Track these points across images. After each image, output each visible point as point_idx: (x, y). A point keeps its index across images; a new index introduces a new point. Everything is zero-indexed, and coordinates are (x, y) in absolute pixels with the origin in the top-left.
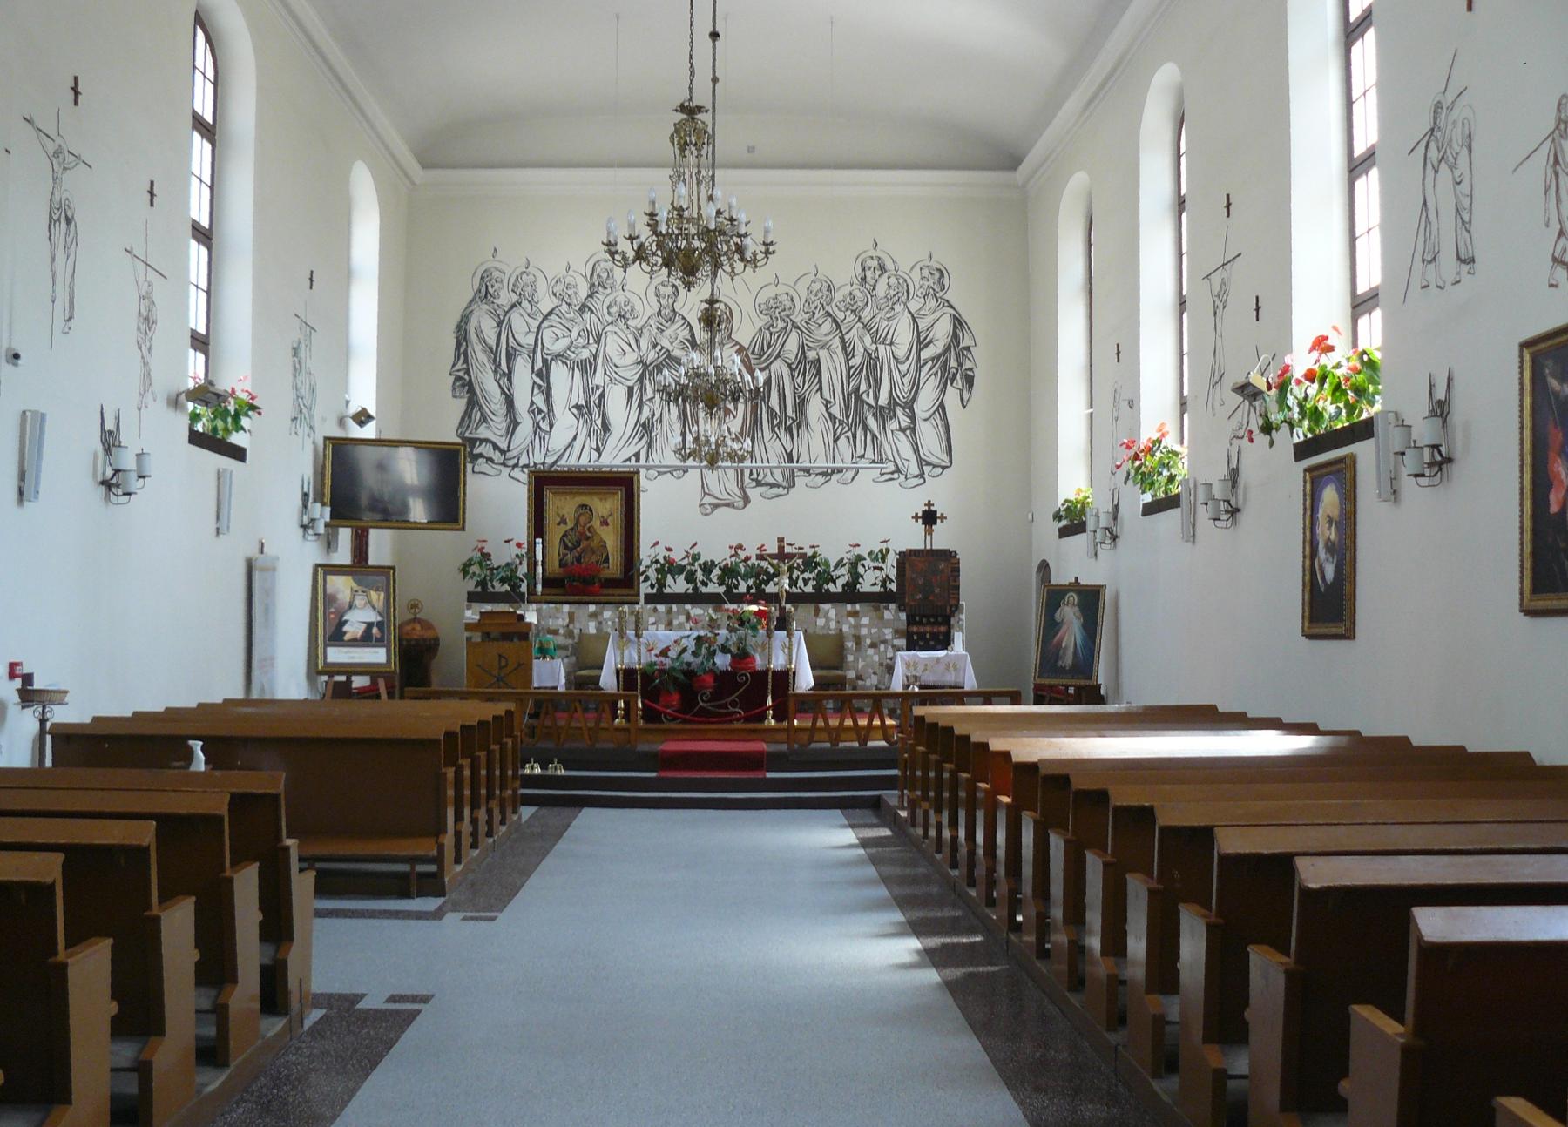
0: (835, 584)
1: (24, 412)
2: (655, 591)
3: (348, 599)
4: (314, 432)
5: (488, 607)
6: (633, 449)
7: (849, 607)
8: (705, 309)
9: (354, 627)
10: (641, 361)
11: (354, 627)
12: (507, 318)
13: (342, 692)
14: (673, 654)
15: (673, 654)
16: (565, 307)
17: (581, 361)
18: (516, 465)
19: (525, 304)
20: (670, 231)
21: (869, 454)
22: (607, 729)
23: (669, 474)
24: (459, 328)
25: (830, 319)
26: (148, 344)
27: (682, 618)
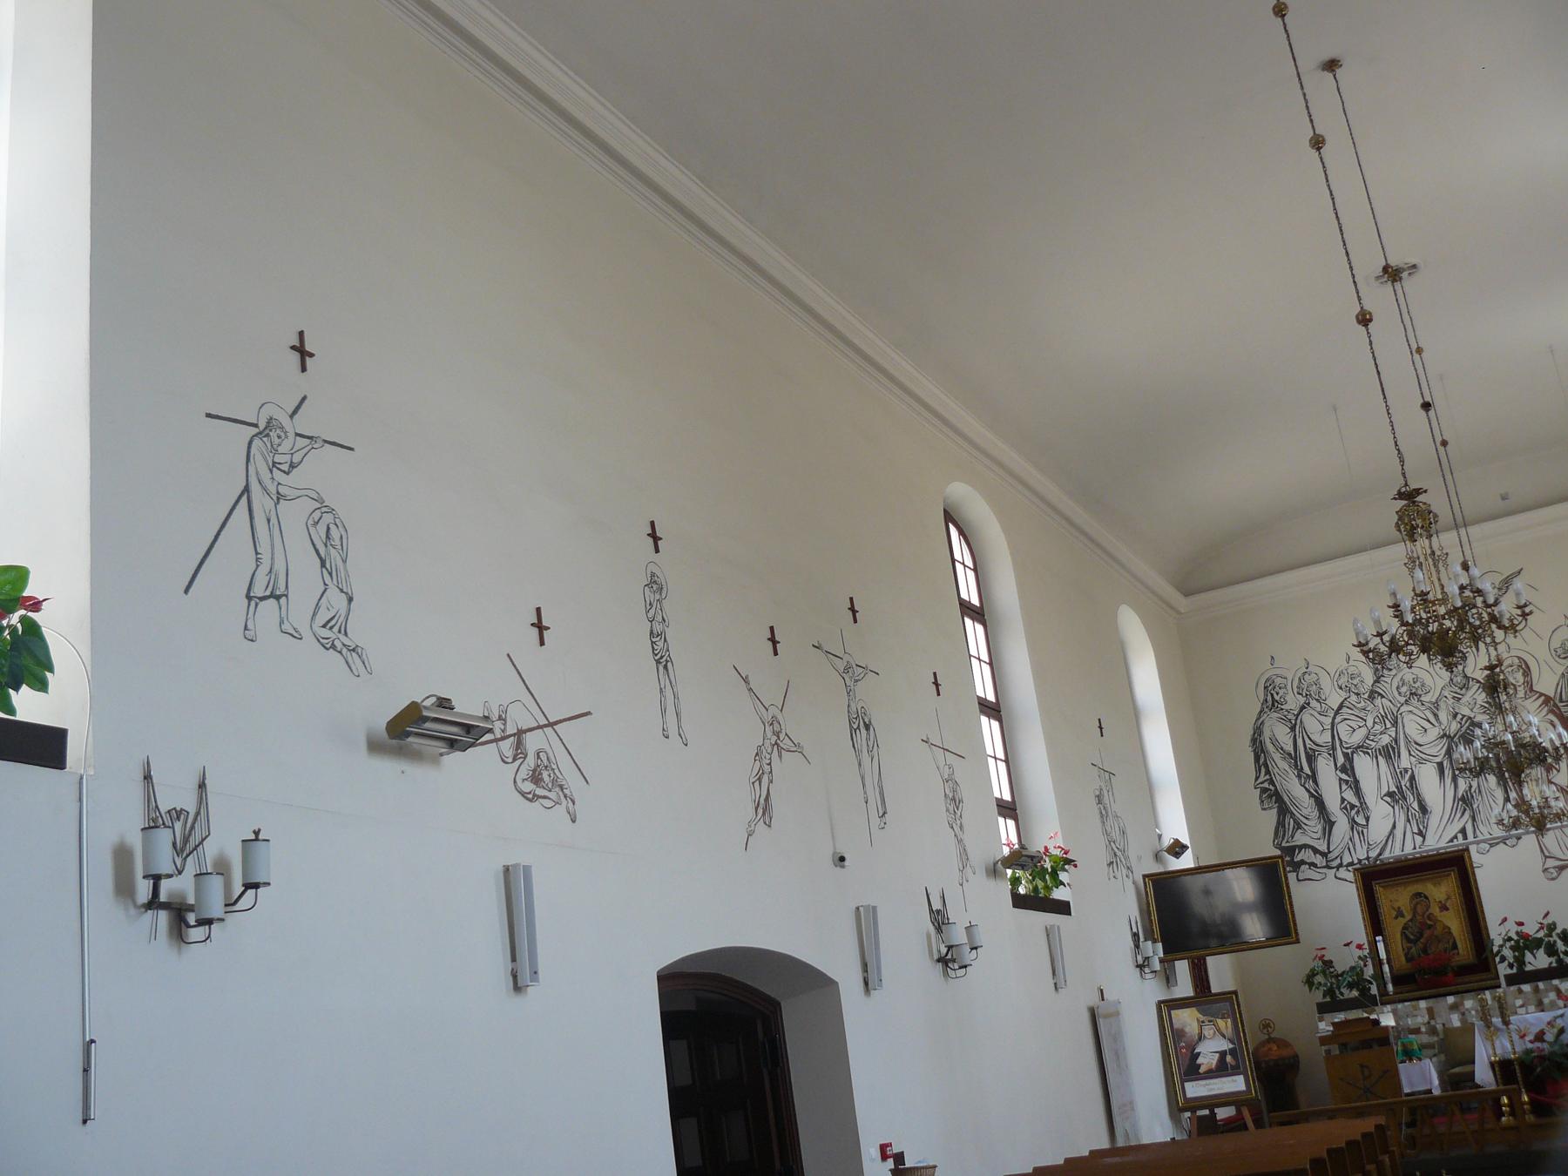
1: (858, 908)
2: (1515, 971)
3: (1196, 1031)
4: (1132, 872)
5: (1340, 1017)
6: (1457, 826)
8: (1487, 676)
9: (1207, 1059)
10: (1445, 735)
11: (1207, 1059)
12: (1298, 721)
13: (1207, 1126)
14: (1549, 1037)
15: (1549, 1037)
16: (1354, 698)
17: (1383, 747)
18: (1341, 865)
19: (1314, 703)
20: (1418, 617)
23: (1502, 844)
24: (1254, 741)
26: (958, 822)
27: (1553, 995)
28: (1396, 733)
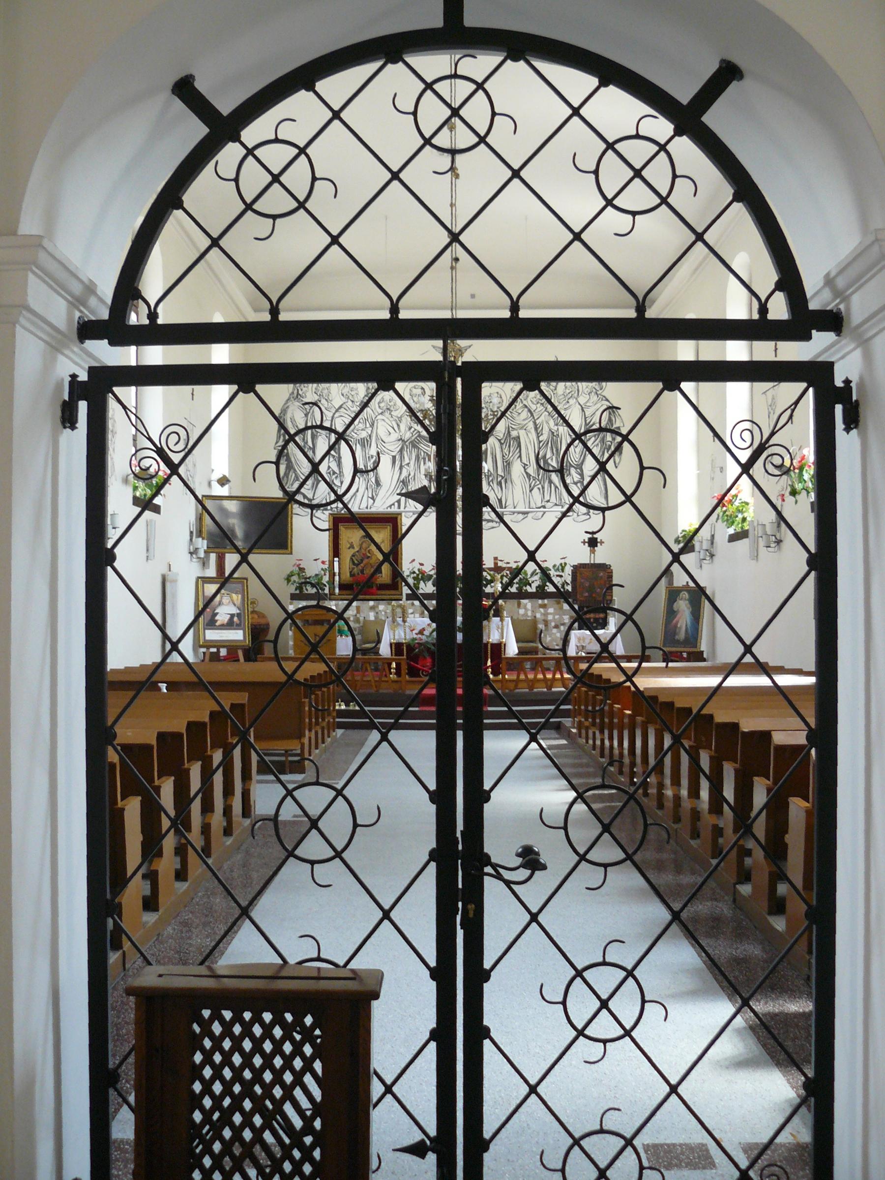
0: (530, 585)
7: (540, 601)
10: (401, 439)
12: (311, 411)
14: (427, 633)
16: (350, 403)
21: (553, 499)
22: (385, 681)
25: (526, 409)
28: (372, 431)
